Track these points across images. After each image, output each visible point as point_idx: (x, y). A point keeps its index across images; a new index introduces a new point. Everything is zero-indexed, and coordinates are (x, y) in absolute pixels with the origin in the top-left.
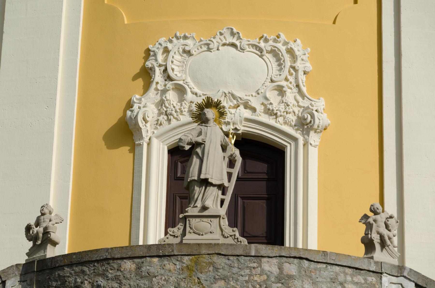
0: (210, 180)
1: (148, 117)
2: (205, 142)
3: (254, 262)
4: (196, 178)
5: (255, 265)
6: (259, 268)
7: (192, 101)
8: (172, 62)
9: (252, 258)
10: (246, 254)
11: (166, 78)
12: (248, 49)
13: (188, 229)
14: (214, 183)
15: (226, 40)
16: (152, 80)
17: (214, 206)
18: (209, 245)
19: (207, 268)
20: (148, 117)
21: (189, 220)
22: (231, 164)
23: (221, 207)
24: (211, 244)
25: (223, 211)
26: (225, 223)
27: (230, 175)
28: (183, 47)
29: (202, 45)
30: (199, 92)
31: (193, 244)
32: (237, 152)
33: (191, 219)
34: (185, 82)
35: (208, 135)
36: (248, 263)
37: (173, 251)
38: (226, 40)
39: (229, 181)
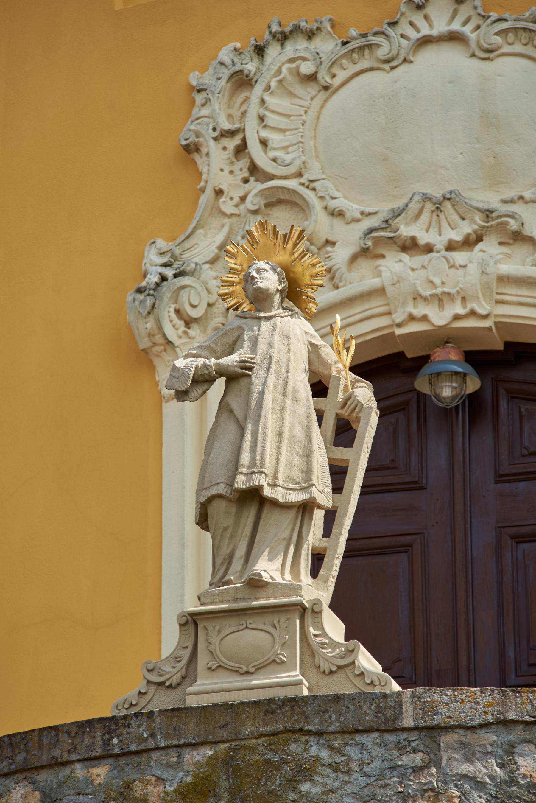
0: (267, 492)
1: (193, 306)
2: (250, 369)
3: (414, 751)
4: (221, 489)
5: (418, 759)
6: (434, 770)
7: (330, 239)
8: (262, 119)
9: (405, 735)
10: (386, 722)
11: (246, 174)
12: (507, 49)
13: (203, 659)
14: (281, 500)
15: (431, 26)
16: (202, 184)
17: (288, 576)
18: (267, 707)
19: (263, 781)
20: (193, 306)
21: (205, 628)
22: (344, 432)
23: (314, 574)
24: (270, 701)
25: (318, 592)
26: (334, 627)
27: (338, 474)
28: (293, 65)
29: (353, 50)
30: (352, 208)
31: (242, 704)
32: (364, 392)
33: (209, 625)
34: (302, 180)
35: (262, 347)
36: (396, 753)
37: (153, 735)
38: (431, 26)
39: (337, 488)
